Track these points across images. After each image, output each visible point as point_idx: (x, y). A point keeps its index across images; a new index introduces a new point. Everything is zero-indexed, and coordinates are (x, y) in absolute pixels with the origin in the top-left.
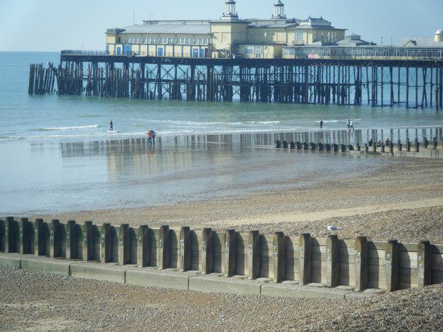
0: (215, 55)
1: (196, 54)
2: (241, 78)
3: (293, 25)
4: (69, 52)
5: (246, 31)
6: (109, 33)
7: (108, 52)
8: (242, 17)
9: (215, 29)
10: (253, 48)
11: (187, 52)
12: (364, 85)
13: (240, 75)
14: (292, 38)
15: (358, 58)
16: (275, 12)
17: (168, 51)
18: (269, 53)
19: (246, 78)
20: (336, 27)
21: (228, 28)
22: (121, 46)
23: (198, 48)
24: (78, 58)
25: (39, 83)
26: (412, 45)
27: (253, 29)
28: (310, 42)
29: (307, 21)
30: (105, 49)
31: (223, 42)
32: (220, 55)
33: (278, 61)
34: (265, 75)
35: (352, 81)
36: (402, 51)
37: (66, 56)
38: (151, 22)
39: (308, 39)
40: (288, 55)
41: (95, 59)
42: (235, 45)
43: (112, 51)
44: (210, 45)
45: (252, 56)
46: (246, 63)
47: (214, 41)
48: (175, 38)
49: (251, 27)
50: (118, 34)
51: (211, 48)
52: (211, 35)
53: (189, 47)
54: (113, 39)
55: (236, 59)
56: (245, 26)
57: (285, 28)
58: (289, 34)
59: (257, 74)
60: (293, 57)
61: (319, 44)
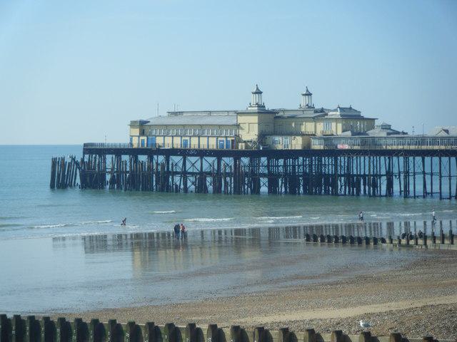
0: (241, 146)
1: (143, 144)
2: (268, 170)
3: (321, 114)
4: (92, 144)
5: (274, 122)
6: (133, 124)
7: (131, 144)
8: (269, 107)
9: (241, 119)
10: (280, 138)
11: (213, 144)
12: (396, 176)
13: (268, 166)
14: (320, 128)
15: (389, 148)
16: (303, 101)
17: (194, 143)
18: (297, 143)
19: (274, 170)
20: (365, 117)
21: (255, 119)
22: (145, 138)
23: (224, 139)
24: (101, 151)
25: (61, 177)
26: (444, 134)
27: (284, 120)
28: (340, 132)
29: (336, 110)
30: (129, 142)
31: (250, 132)
32: (246, 146)
33: (307, 152)
34: (294, 167)
35: (383, 172)
36: (434, 140)
37: (88, 149)
38: (176, 114)
39: (337, 129)
40: (317, 145)
41: (118, 152)
42: (262, 136)
43: (136, 143)
44: (237, 136)
45: (280, 147)
46: (273, 154)
47: (241, 132)
48: (201, 130)
49: (279, 117)
50: (142, 126)
51: (237, 139)
52: (238, 126)
53: (215, 139)
54: (136, 132)
55: (263, 150)
56: (271, 116)
57: (314, 118)
58: (318, 124)
59: (285, 166)
60: (322, 147)
61: (349, 133)
